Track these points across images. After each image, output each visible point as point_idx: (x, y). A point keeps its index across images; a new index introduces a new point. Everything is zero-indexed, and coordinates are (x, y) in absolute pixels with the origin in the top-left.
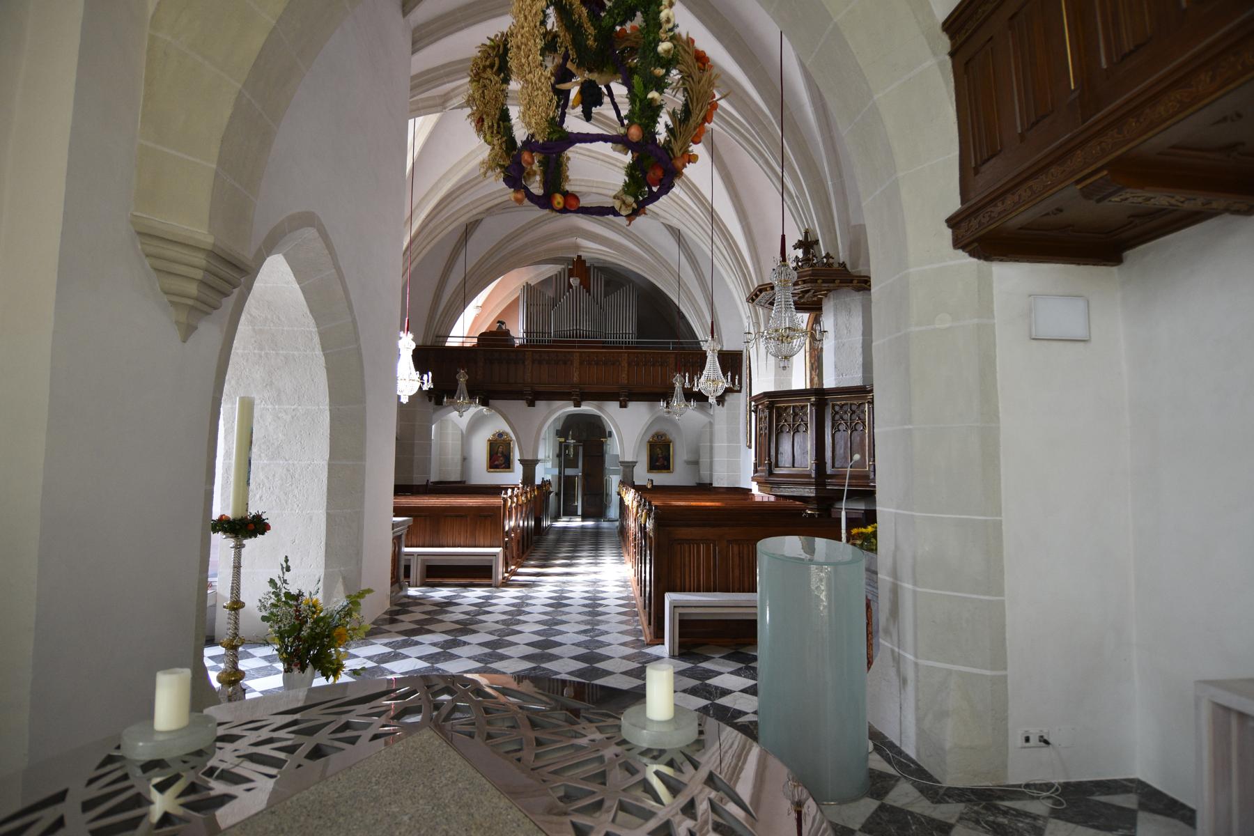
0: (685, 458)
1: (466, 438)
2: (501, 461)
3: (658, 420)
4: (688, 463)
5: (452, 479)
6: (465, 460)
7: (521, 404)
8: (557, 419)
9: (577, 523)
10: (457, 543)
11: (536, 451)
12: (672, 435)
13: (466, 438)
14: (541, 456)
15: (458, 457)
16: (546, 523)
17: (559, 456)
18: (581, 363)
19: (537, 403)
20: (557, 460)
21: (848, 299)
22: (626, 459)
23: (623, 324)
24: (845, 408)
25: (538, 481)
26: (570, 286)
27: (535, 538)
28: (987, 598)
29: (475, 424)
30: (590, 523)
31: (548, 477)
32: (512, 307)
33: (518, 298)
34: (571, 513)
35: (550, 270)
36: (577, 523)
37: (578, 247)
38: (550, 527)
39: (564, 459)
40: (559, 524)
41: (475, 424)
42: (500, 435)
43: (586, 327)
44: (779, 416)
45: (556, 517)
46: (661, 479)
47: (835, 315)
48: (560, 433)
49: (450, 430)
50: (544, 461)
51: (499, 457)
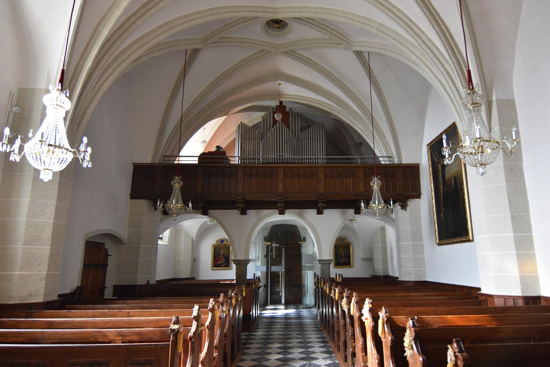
1: (196, 244)
2: (222, 261)
3: (345, 228)
4: (364, 260)
5: (183, 276)
6: (195, 261)
7: (235, 213)
8: (263, 229)
9: (281, 311)
11: (247, 252)
12: (351, 239)
13: (196, 244)
14: (252, 256)
15: (189, 259)
16: (255, 312)
17: (266, 256)
18: (285, 176)
20: (265, 260)
22: (324, 258)
23: (317, 154)
25: (250, 276)
26: (275, 122)
27: (244, 335)
29: (203, 232)
30: (291, 311)
31: (258, 274)
33: (234, 141)
34: (276, 301)
35: (257, 117)
36: (281, 311)
37: (279, 94)
38: (260, 317)
39: (271, 259)
40: (268, 313)
42: (222, 241)
43: (287, 155)
45: (264, 307)
46: (347, 272)
48: (266, 239)
49: (183, 238)
50: (255, 260)
51: (221, 258)
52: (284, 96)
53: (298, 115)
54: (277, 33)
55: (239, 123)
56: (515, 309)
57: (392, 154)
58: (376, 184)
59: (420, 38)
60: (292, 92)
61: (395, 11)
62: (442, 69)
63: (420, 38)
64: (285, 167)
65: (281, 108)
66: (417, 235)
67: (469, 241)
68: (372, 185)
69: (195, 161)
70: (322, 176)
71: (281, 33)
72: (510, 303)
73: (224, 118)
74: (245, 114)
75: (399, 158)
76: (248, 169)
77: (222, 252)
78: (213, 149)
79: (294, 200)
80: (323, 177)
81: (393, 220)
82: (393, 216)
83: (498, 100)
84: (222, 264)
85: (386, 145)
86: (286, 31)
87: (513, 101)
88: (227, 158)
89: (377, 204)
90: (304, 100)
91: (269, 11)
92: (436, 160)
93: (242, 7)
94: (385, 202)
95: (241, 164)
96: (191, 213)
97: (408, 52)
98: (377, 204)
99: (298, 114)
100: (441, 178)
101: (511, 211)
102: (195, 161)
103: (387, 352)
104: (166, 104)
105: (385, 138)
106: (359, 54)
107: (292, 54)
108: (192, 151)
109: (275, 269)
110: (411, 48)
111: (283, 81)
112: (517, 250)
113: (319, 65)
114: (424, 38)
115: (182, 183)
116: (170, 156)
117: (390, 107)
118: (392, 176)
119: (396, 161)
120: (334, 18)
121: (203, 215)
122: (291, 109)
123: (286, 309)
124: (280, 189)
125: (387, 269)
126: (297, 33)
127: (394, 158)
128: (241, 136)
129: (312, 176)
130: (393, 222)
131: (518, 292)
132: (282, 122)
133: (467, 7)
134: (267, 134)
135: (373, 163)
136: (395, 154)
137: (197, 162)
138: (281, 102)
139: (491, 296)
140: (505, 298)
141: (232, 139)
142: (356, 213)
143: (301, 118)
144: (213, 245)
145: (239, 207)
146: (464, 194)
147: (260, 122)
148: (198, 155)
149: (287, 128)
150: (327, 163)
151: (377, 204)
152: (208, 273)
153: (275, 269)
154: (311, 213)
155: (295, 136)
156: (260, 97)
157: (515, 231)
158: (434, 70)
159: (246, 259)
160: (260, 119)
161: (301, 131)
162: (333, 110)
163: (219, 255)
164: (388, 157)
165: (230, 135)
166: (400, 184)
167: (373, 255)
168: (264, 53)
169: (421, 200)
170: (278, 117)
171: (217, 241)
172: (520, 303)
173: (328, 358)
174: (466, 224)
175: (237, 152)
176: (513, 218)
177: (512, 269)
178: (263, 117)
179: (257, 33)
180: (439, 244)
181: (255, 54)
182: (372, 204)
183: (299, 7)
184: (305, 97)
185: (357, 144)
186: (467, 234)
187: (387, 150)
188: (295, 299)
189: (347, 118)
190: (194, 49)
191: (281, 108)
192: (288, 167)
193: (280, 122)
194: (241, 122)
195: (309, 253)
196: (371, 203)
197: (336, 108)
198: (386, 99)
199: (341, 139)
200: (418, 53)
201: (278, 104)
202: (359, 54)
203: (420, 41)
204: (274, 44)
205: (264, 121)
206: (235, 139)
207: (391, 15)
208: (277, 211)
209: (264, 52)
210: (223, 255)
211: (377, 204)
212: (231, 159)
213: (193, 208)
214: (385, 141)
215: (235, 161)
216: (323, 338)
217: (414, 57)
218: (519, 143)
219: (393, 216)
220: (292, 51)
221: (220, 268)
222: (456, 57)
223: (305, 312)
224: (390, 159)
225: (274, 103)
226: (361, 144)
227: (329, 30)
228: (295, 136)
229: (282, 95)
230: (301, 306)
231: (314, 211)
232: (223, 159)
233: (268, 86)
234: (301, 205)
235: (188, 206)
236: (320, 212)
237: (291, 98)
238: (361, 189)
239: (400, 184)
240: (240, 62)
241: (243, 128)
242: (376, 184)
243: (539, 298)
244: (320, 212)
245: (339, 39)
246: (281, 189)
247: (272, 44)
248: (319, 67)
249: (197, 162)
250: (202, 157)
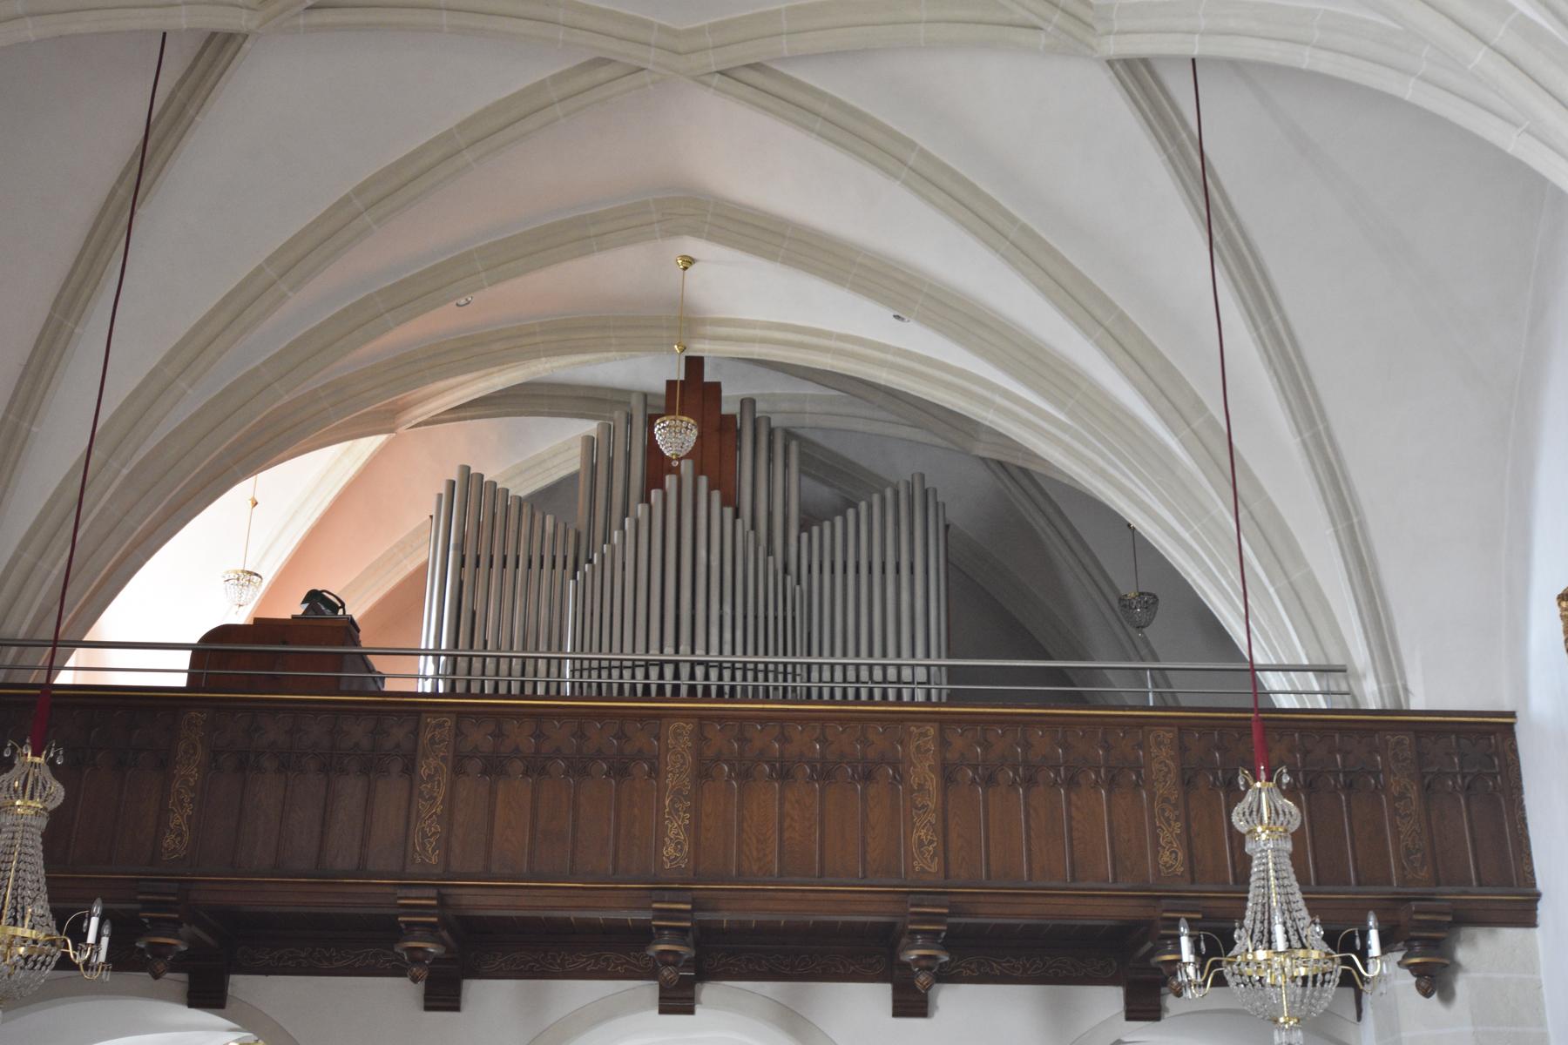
18: (703, 772)
23: (896, 650)
26: (657, 466)
37: (684, 319)
43: (717, 649)
52: (710, 330)
55: (455, 476)
57: (1345, 651)
58: (1266, 821)
60: (754, 307)
64: (702, 718)
65: (694, 391)
68: (1241, 825)
69: (172, 671)
70: (924, 773)
73: (367, 446)
74: (487, 428)
75: (1391, 678)
76: (485, 729)
78: (291, 607)
79: (753, 918)
80: (933, 783)
85: (1305, 601)
88: (362, 660)
89: (1279, 947)
90: (826, 350)
94: (1329, 938)
95: (452, 692)
96: (98, 990)
98: (1281, 944)
99: (789, 434)
102: (172, 671)
106: (1137, 74)
108: (156, 619)
111: (711, 237)
113: (911, 145)
115: (57, 792)
116: (24, 644)
118: (1349, 786)
119: (1371, 695)
121: (191, 1005)
122: (748, 403)
124: (669, 851)
127: (1359, 678)
128: (461, 547)
129: (868, 777)
132: (698, 471)
134: (607, 538)
135: (1247, 702)
136: (1360, 655)
137: (181, 681)
138: (694, 365)
141: (410, 566)
142: (1132, 1014)
143: (804, 459)
145: (417, 957)
147: (572, 479)
148: (194, 639)
149: (724, 503)
150: (954, 698)
151: (1281, 944)
155: (770, 551)
160: (571, 463)
161: (804, 526)
162: (986, 403)
164: (1319, 670)
170: (676, 437)
175: (430, 630)
178: (589, 442)
181: (558, 79)
182: (1249, 953)
184: (828, 335)
185: (1125, 604)
190: (214, 34)
191: (694, 391)
192: (721, 718)
193: (687, 467)
196: (1242, 939)
197: (1006, 394)
198: (1300, 334)
199: (1025, 565)
201: (679, 374)
202: (1137, 74)
204: (662, 29)
205: (594, 470)
206: (422, 571)
209: (603, 74)
211: (1279, 947)
212: (380, 664)
213: (121, 960)
214: (1296, 576)
215: (423, 676)
217: (1480, 57)
220: (756, 67)
224: (1335, 682)
225: (653, 371)
226: (1154, 598)
228: (770, 551)
229: (703, 322)
231: (874, 997)
232: (338, 661)
233: (623, 270)
235: (79, 936)
237: (752, 340)
238: (1166, 857)
241: (470, 496)
242: (1266, 821)
247: (647, 25)
248: (912, 159)
249: (181, 681)
250: (217, 651)
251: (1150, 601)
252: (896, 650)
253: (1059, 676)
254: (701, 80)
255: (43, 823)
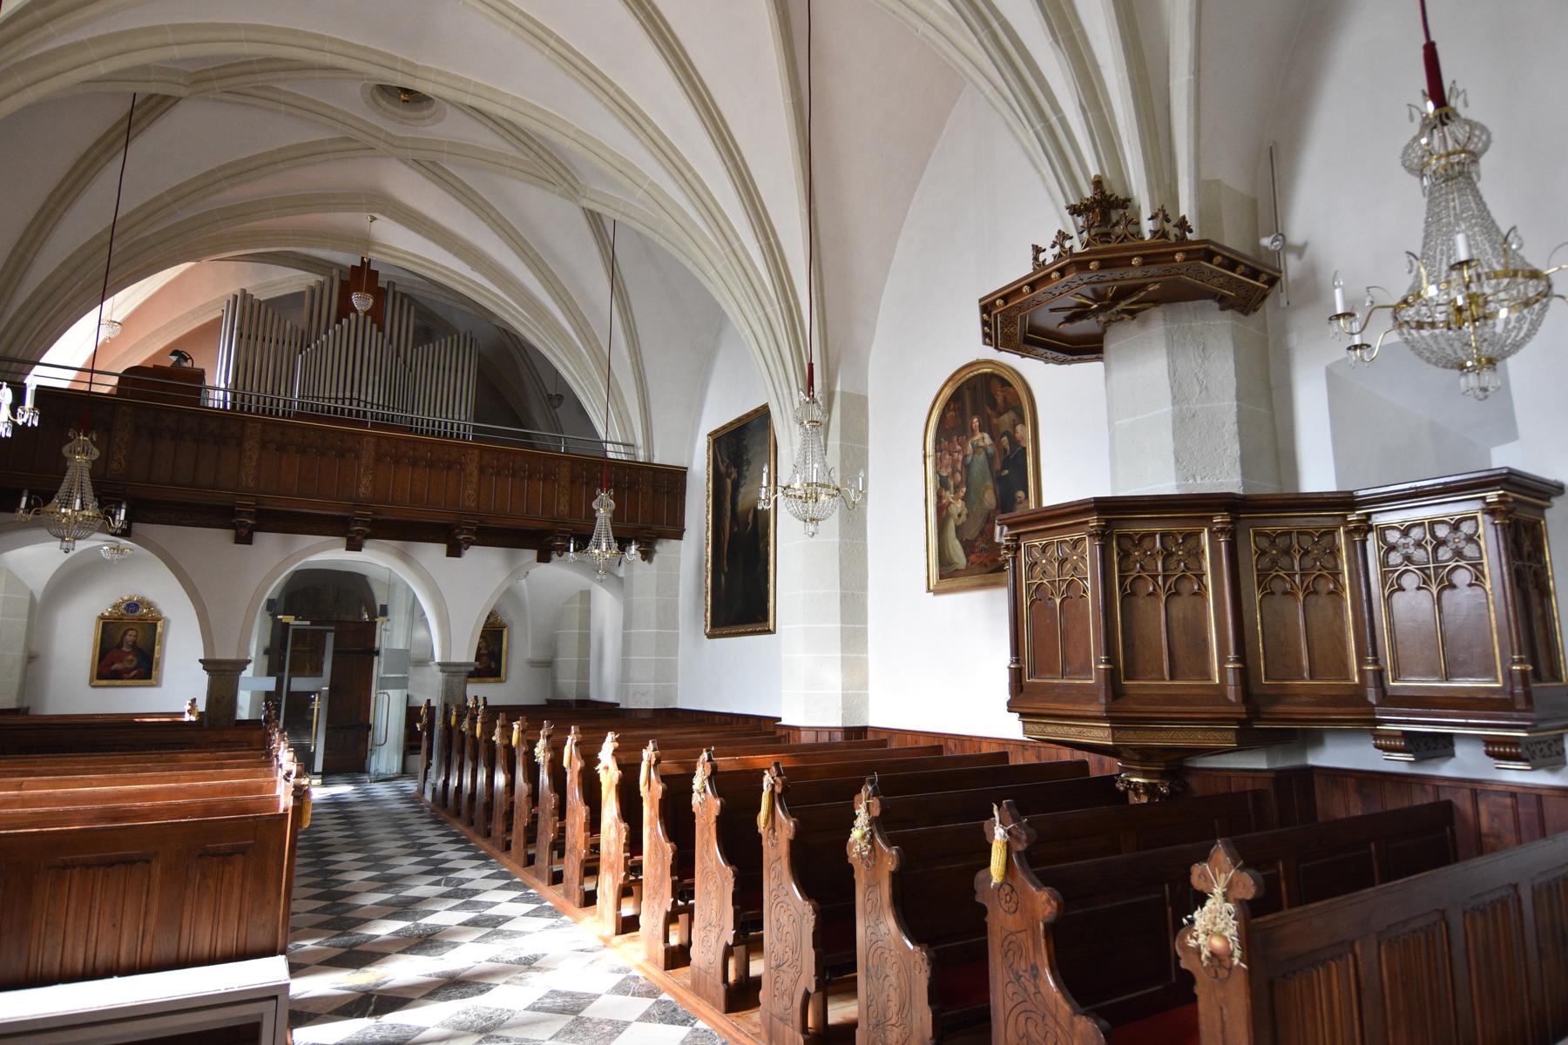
0: (529, 655)
2: (130, 660)
3: (510, 594)
4: (534, 664)
7: (219, 538)
10: (49, 959)
12: (509, 616)
19: (259, 537)
21: (1197, 324)
22: (454, 659)
23: (451, 408)
24: (1416, 533)
28: (1284, 897)
29: (66, 583)
30: (343, 790)
32: (209, 331)
35: (291, 280)
37: (366, 241)
41: (66, 583)
43: (372, 399)
44: (1125, 555)
47: (1170, 354)
53: (407, 298)
54: (400, 112)
56: (830, 746)
59: (730, 244)
60: (398, 245)
61: (689, 176)
62: (760, 313)
63: (730, 244)
66: (667, 616)
67: (768, 632)
68: (594, 506)
70: (473, 469)
71: (414, 114)
72: (824, 738)
77: (129, 638)
81: (621, 580)
82: (621, 572)
83: (843, 393)
84: (129, 671)
86: (425, 113)
87: (866, 399)
91: (399, 67)
92: (723, 468)
93: (332, 40)
97: (701, 258)
99: (404, 295)
100: (728, 505)
101: (842, 587)
103: (649, 812)
104: (32, 215)
105: (623, 403)
106: (594, 219)
107: (431, 169)
109: (300, 684)
110: (709, 253)
112: (842, 651)
114: (736, 245)
115: (96, 453)
117: (641, 341)
119: (641, 456)
120: (555, 137)
123: (324, 784)
125: (587, 686)
126: (448, 128)
128: (240, 328)
129: (449, 468)
130: (619, 584)
131: (836, 721)
133: (820, 260)
134: (318, 337)
136: (640, 441)
139: (797, 729)
140: (817, 730)
144: (102, 617)
146: (767, 544)
152: (73, 690)
153: (300, 684)
154: (432, 554)
156: (309, 236)
157: (843, 620)
158: (744, 306)
159: (242, 657)
161: (416, 344)
163: (120, 646)
165: (192, 313)
166: (648, 505)
167: (555, 654)
168: (350, 146)
169: (683, 543)
171: (115, 607)
172: (839, 737)
173: (483, 866)
174: (767, 601)
176: (843, 597)
177: (833, 680)
179: (351, 101)
180: (710, 636)
181: (331, 141)
183: (476, 85)
185: (550, 396)
186: (766, 619)
187: (623, 429)
188: (348, 758)
189: (538, 338)
194: (244, 291)
195: (395, 647)
199: (511, 378)
200: (719, 267)
203: (728, 250)
207: (682, 181)
208: (343, 541)
210: (134, 646)
211: (602, 549)
215: (217, 398)
216: (454, 834)
217: (712, 273)
218: (865, 496)
219: (621, 572)
221: (118, 682)
222: (787, 301)
223: (381, 790)
226: (561, 398)
227: (535, 147)
230: (365, 777)
231: (439, 550)
234: (404, 529)
236: (454, 551)
239: (648, 505)
240: (280, 151)
243: (865, 729)
244: (454, 551)
245: (553, 174)
246: (364, 490)
251: (560, 398)
252: (451, 408)
253: (528, 436)
254: (403, 161)
255: (89, 466)
